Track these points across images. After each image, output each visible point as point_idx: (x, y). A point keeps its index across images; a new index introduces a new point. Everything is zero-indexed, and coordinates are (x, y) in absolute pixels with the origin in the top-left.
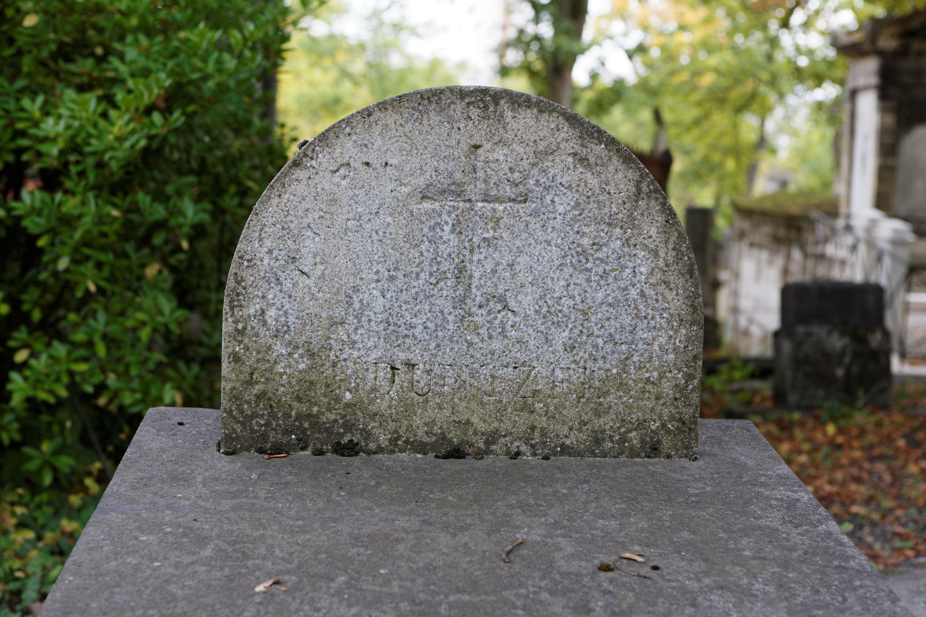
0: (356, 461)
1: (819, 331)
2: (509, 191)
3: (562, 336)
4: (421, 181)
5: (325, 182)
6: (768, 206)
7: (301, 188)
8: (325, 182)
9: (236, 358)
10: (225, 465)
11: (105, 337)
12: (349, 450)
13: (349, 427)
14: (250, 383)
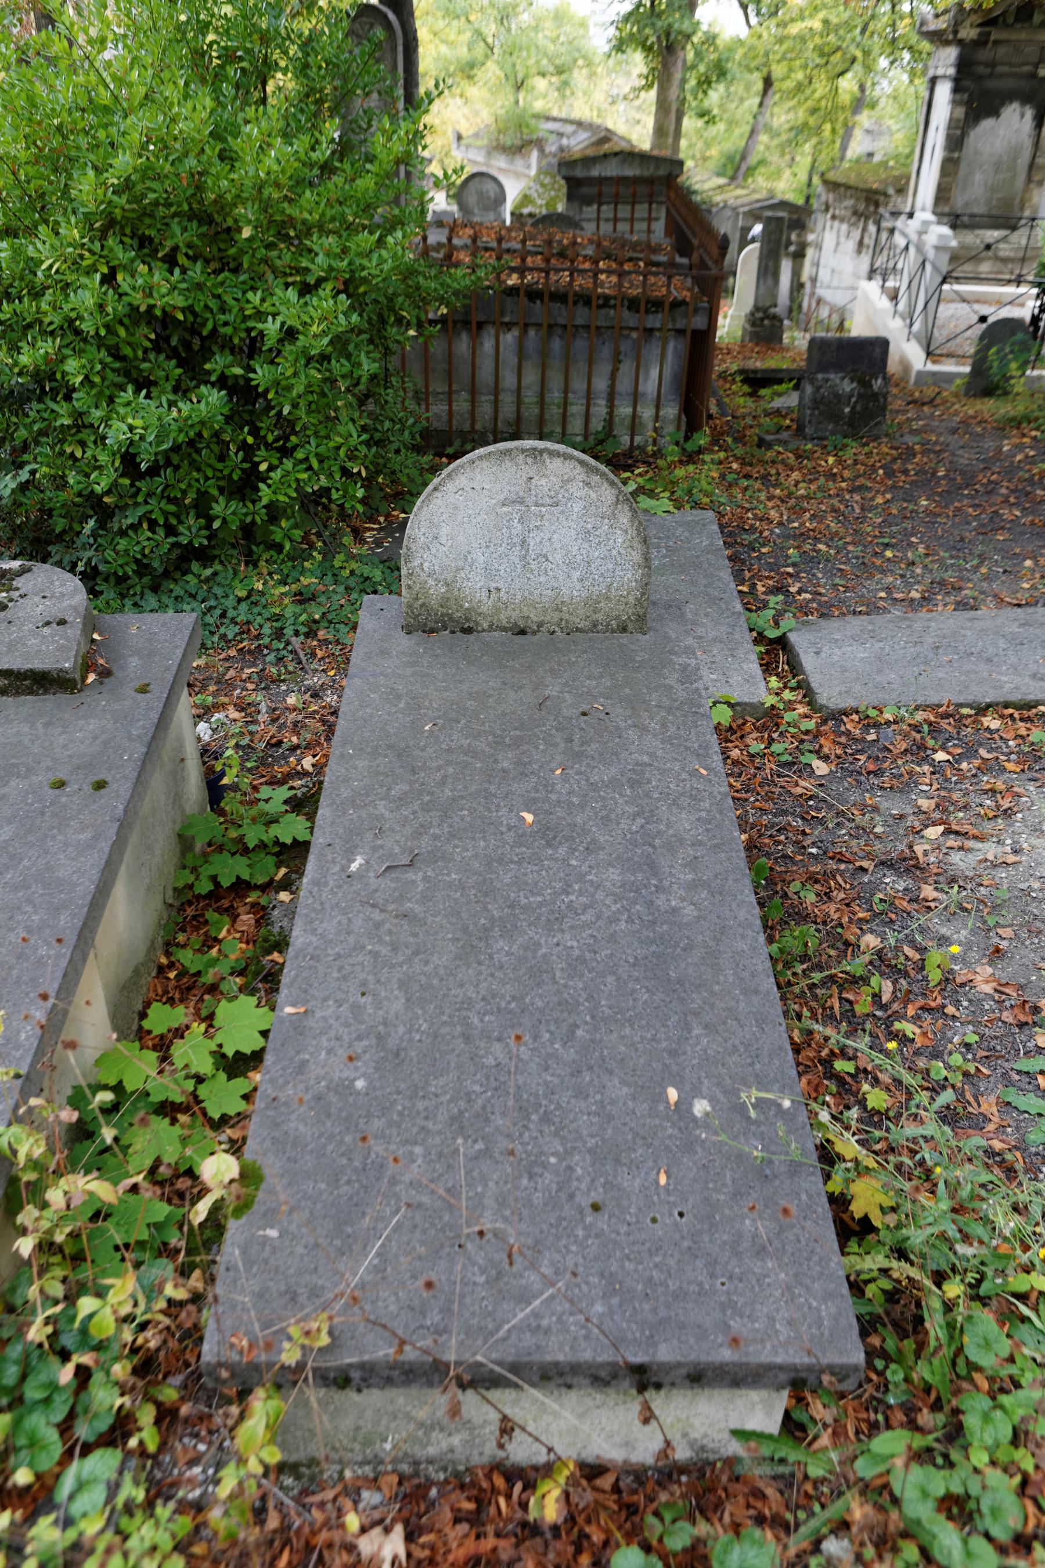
0: (471, 637)
1: (834, 377)
2: (548, 501)
3: (576, 575)
4: (502, 497)
5: (451, 498)
6: (853, 180)
7: (438, 502)
8: (451, 498)
9: (409, 587)
10: (404, 642)
11: (317, 455)
12: (468, 631)
13: (467, 620)
14: (417, 599)
